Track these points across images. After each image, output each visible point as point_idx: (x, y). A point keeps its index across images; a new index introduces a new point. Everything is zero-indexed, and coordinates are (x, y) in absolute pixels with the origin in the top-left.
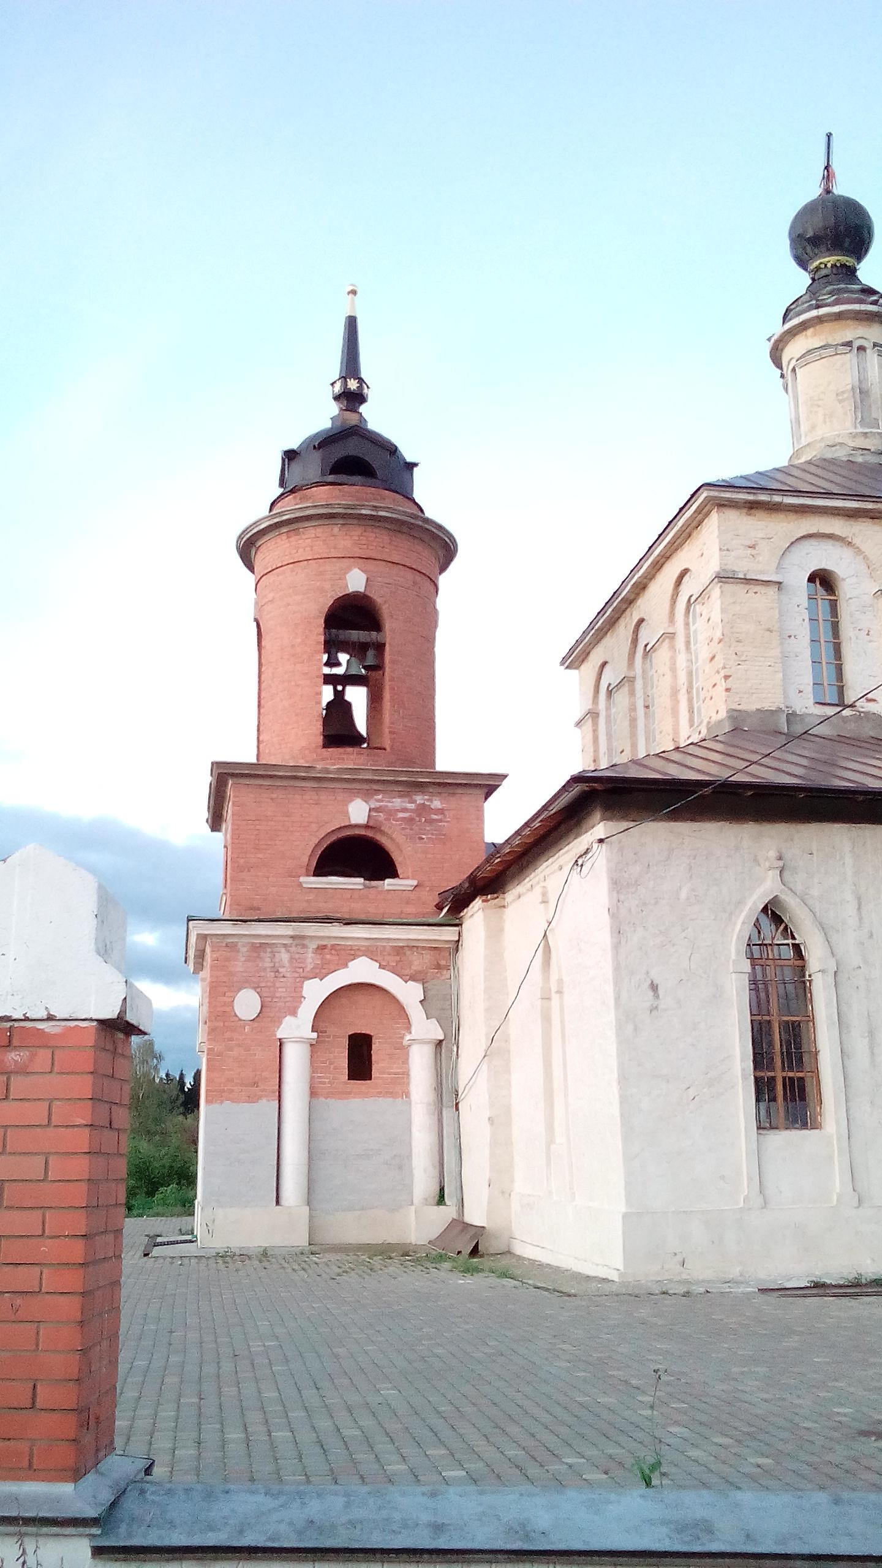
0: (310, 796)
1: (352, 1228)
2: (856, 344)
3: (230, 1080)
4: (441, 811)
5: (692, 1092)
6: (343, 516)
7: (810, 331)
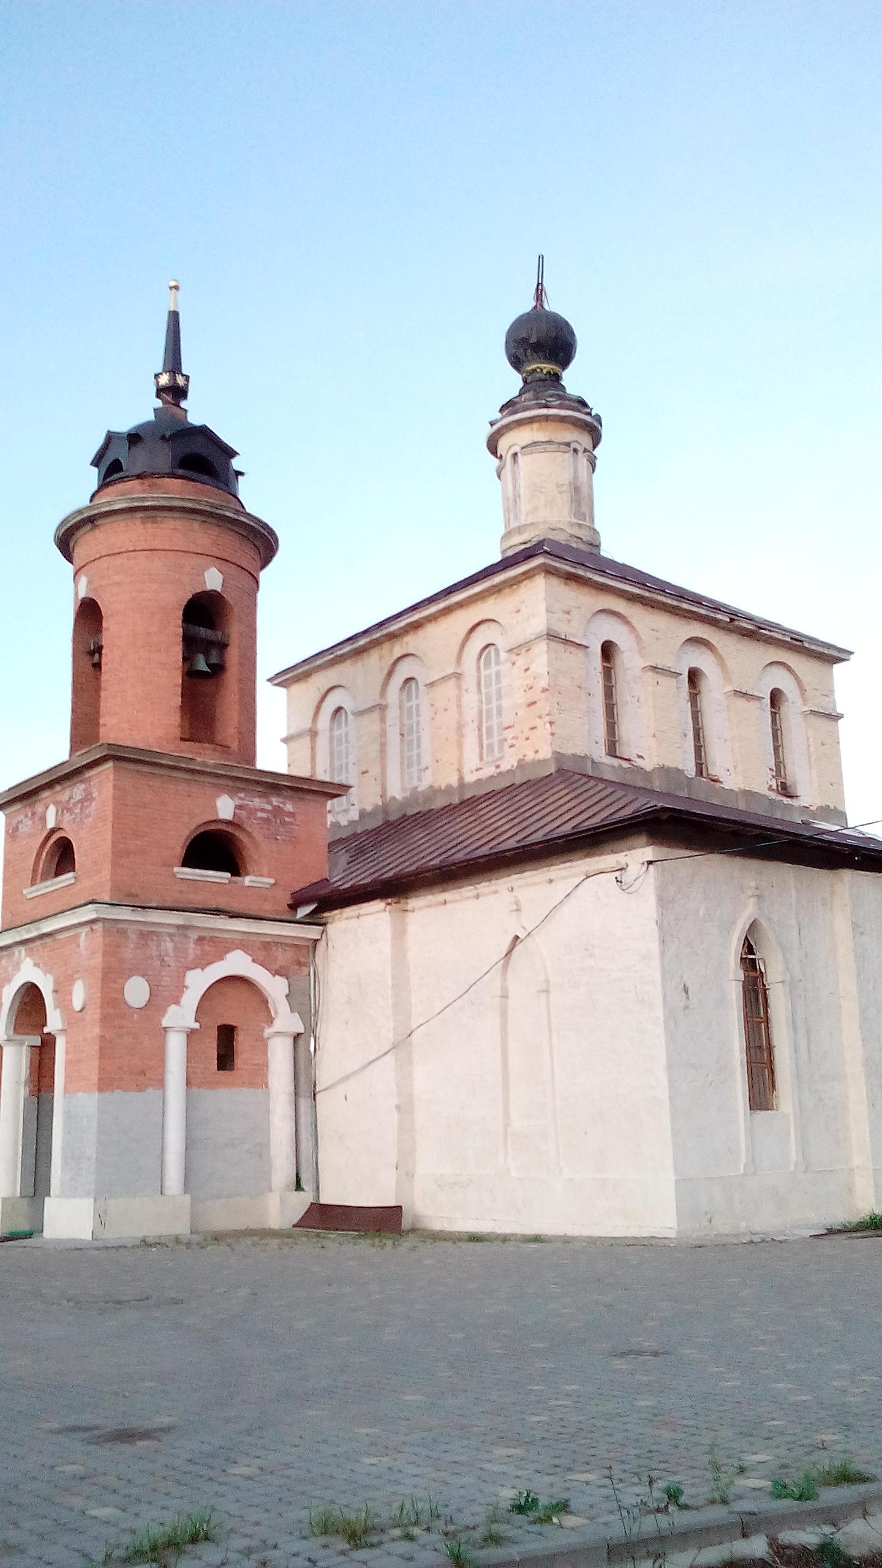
0: (182, 787)
1: (221, 1219)
2: (573, 446)
3: (120, 1068)
4: (292, 815)
5: (710, 1078)
6: (211, 515)
7: (535, 426)
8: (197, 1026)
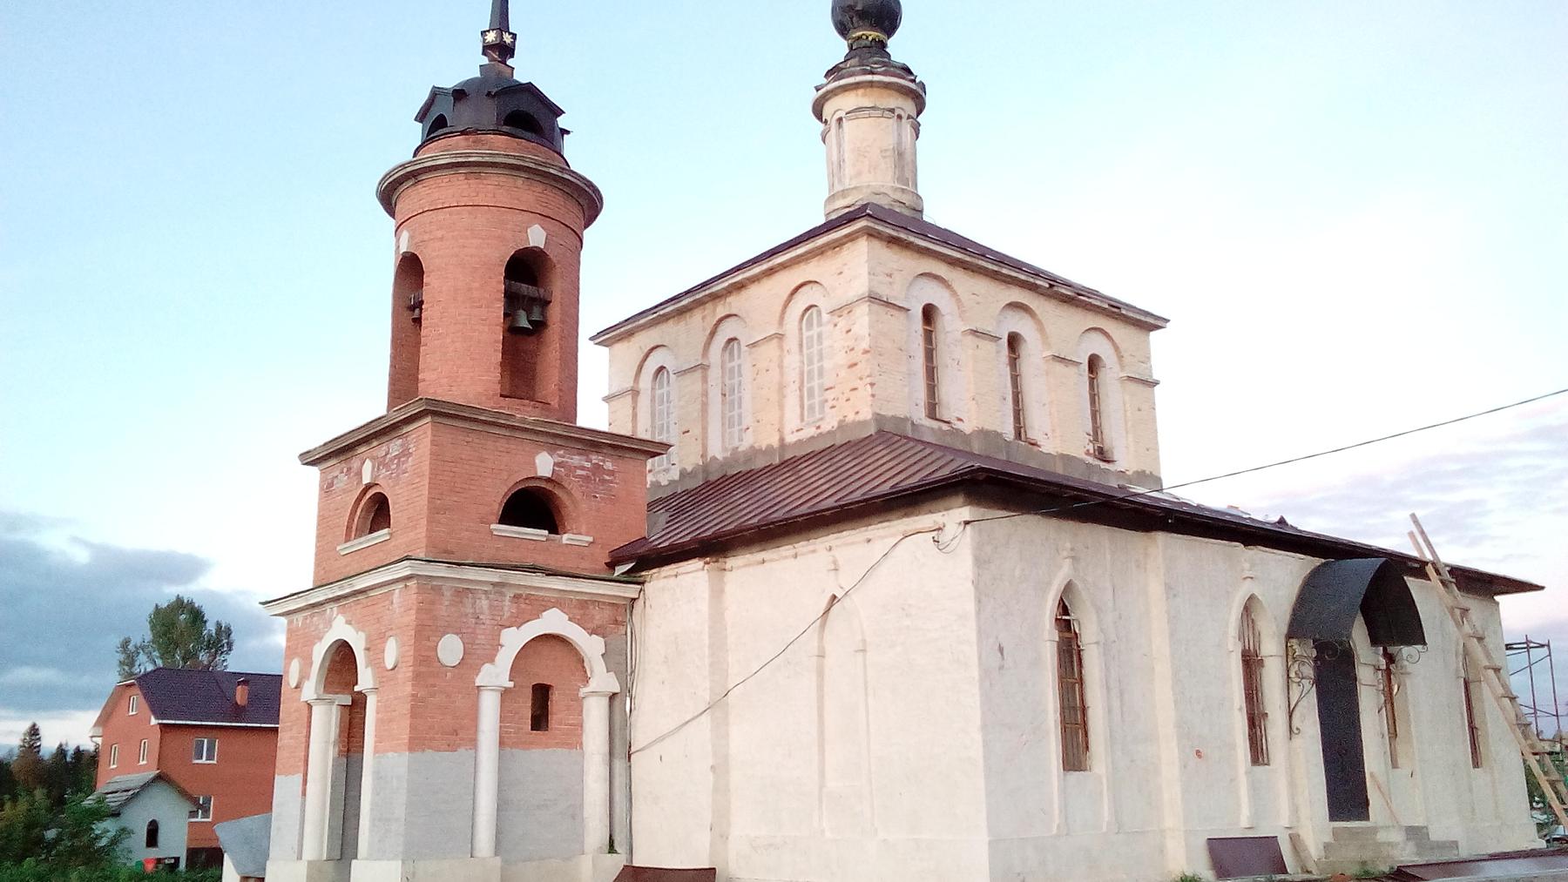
4: (612, 473)
7: (860, 91)
8: (511, 684)
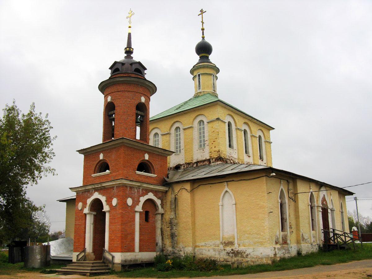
8: (142, 211)
